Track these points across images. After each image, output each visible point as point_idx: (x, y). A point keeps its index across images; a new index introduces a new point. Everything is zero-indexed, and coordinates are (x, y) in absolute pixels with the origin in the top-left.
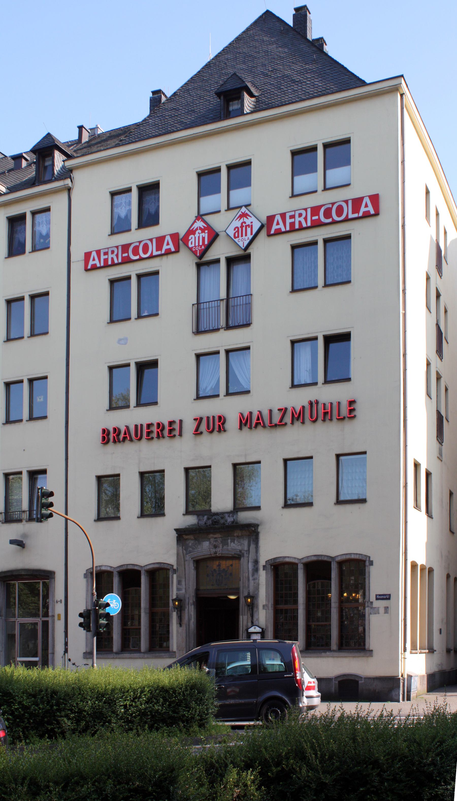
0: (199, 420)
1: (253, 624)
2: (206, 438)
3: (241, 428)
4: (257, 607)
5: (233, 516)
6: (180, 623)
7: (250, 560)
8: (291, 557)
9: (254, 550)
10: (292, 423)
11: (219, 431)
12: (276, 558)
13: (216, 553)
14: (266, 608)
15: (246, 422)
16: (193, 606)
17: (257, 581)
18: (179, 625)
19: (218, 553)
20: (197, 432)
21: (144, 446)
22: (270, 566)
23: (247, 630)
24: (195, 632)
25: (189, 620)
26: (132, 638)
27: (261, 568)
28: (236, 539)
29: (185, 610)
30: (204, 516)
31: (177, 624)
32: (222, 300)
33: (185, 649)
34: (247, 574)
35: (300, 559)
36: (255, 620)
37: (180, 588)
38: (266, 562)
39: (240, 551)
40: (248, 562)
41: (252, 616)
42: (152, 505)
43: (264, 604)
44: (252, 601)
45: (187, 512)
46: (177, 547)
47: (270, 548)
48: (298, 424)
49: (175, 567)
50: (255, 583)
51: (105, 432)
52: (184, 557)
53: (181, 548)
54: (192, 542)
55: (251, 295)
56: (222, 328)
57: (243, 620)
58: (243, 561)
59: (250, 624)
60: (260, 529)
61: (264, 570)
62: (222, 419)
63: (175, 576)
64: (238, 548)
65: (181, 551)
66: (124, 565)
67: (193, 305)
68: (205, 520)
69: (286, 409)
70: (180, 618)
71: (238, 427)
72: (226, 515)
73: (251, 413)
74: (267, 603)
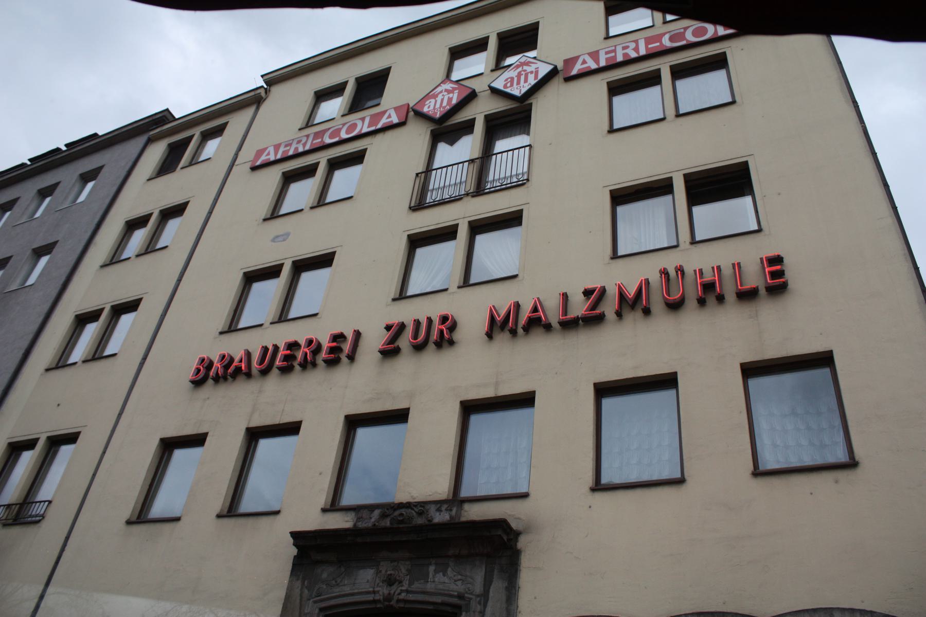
0: (396, 331)
2: (406, 363)
3: (490, 335)
5: (451, 510)
10: (619, 314)
11: (439, 345)
13: (388, 598)
15: (501, 326)
19: (396, 598)
20: (390, 352)
21: (273, 385)
39: (461, 596)
46: (290, 582)
48: (633, 319)
52: (300, 608)
53: (298, 584)
60: (522, 542)
62: (449, 323)
64: (455, 587)
65: (297, 591)
67: (417, 175)
68: (373, 520)
69: (603, 291)
72: (432, 509)
73: (517, 306)
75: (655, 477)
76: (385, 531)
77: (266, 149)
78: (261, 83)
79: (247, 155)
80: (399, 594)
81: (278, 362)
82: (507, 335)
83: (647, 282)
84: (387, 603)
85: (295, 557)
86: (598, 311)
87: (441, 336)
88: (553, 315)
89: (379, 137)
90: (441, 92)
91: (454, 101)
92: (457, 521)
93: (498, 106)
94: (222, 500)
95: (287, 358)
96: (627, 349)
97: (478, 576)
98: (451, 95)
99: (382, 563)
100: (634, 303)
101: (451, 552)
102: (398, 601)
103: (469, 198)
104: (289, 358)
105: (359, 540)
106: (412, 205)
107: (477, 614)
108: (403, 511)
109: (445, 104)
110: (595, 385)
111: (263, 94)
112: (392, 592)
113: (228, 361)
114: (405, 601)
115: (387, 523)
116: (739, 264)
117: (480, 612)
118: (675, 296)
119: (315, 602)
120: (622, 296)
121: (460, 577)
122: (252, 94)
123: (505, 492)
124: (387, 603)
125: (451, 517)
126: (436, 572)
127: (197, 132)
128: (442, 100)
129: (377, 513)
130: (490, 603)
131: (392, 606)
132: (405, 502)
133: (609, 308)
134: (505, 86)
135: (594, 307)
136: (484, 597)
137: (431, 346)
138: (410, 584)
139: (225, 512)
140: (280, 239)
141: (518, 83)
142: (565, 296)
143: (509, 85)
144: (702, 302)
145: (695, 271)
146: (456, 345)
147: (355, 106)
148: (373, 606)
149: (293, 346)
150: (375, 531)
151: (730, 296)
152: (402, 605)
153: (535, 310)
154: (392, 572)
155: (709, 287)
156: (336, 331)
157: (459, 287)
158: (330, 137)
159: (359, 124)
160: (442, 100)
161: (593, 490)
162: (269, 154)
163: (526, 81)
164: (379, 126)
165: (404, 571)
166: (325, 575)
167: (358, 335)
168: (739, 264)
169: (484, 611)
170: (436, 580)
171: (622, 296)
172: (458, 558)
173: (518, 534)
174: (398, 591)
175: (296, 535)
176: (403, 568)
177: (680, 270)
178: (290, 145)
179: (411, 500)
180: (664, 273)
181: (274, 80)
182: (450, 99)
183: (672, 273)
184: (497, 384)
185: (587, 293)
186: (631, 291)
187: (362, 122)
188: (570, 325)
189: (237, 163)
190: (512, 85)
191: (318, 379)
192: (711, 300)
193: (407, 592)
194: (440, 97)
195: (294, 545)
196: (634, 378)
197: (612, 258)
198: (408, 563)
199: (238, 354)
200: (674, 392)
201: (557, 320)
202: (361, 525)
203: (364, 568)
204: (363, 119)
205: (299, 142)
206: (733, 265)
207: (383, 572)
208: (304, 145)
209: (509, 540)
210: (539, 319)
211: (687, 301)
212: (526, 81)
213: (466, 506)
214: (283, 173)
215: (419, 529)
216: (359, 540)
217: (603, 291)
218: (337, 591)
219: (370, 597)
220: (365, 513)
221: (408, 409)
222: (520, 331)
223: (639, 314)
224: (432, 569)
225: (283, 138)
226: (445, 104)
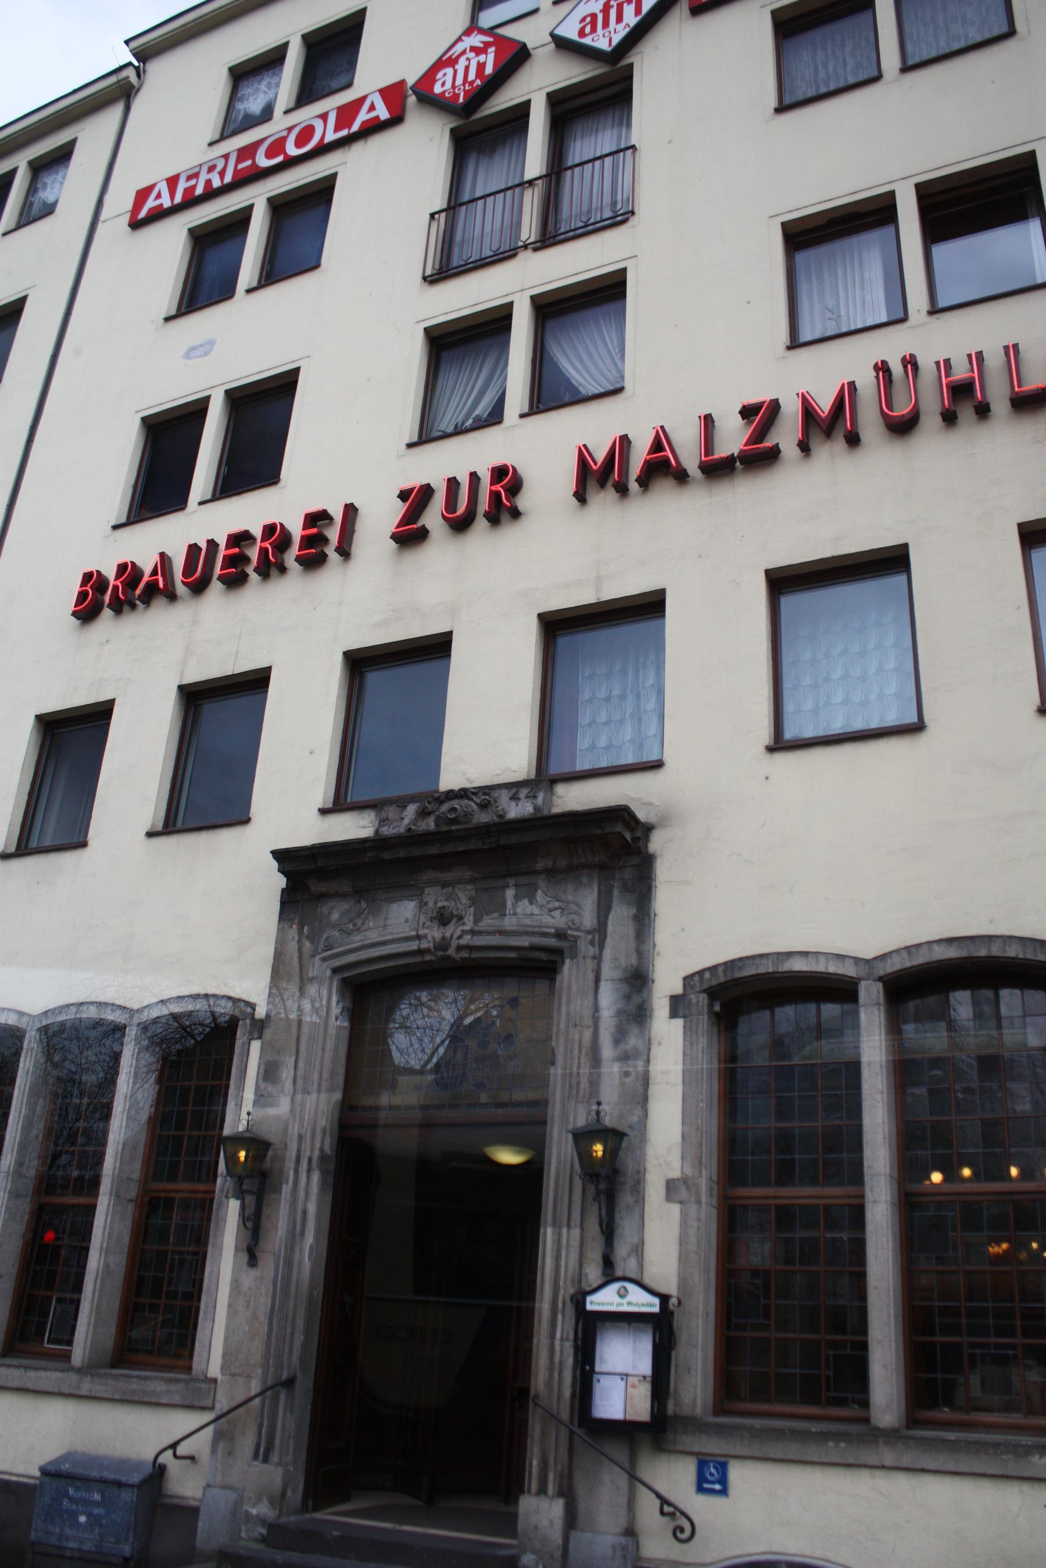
0: (416, 499)
1: (610, 1276)
2: (441, 550)
3: (581, 496)
4: (638, 1188)
5: (535, 797)
6: (251, 1252)
7: (607, 971)
8: (817, 954)
9: (630, 929)
10: (805, 447)
11: (494, 519)
12: (741, 959)
13: (443, 945)
14: (683, 1194)
15: (599, 476)
16: (316, 1177)
17: (640, 1064)
18: (245, 1257)
19: (454, 944)
20: (409, 536)
22: (704, 999)
23: (579, 1300)
24: (319, 1292)
25: (294, 1236)
26: (59, 1301)
27: (661, 1008)
28: (542, 884)
29: (278, 1190)
30: (404, 807)
31: (237, 1249)
32: (531, 183)
33: (259, 1371)
34: (588, 1034)
35: (867, 962)
36: (621, 1250)
37: (271, 1102)
38: (687, 980)
39: (560, 935)
40: (597, 980)
41: (609, 1232)
42: (207, 788)
43: (676, 1174)
44: (612, 1153)
45: (340, 803)
46: (281, 931)
47: (709, 914)
48: (830, 454)
49: (261, 1012)
50: (627, 1074)
51: (93, 582)
53: (293, 932)
54: (344, 906)
55: (633, 147)
56: (525, 247)
57: (561, 1248)
58: (571, 975)
59: (593, 1273)
60: (656, 843)
61: (674, 1015)
62: (507, 480)
63: (256, 1046)
64: (550, 921)
65: (292, 946)
66: (68, 1006)
67: (432, 216)
68: (406, 821)
69: (774, 407)
70: (254, 1227)
71: (572, 487)
72: (504, 796)
73: (625, 441)
74: (689, 1171)
75: (874, 724)
76: (427, 837)
77: (151, 188)
78: (126, 56)
79: (120, 201)
80: (460, 937)
81: (217, 571)
82: (610, 494)
83: (852, 385)
84: (440, 953)
85: (283, 891)
86: (768, 443)
87: (501, 498)
88: (688, 452)
89: (358, 149)
90: (464, 52)
91: (489, 70)
92: (546, 813)
93: (569, 73)
94: (152, 808)
95: (231, 561)
96: (819, 507)
97: (586, 901)
98: (482, 58)
99: (427, 891)
100: (831, 425)
101: (540, 865)
102: (460, 948)
103: (529, 253)
104: (236, 561)
105: (387, 856)
106: (428, 272)
107: (589, 961)
108: (455, 803)
109: (472, 76)
110: (768, 572)
111: (133, 79)
112: (448, 934)
113: (129, 572)
114: (471, 948)
115: (429, 824)
116: (1016, 346)
117: (594, 957)
118: (902, 409)
119: (324, 960)
120: (808, 412)
121: (557, 904)
122: (113, 79)
123: (623, 762)
124: (440, 953)
125: (536, 808)
126: (517, 898)
127: (21, 161)
128: (467, 68)
129: (412, 809)
130: (609, 942)
131: (449, 956)
132: (456, 788)
133: (786, 435)
134: (582, 33)
135: (759, 436)
136: (600, 931)
137: (481, 523)
138: (476, 922)
139: (160, 827)
140: (197, 353)
141: (606, 24)
142: (708, 421)
143: (588, 30)
144: (949, 418)
145: (938, 363)
146: (523, 518)
147: (307, 93)
148: (418, 959)
149: (241, 539)
150: (412, 838)
151: (1000, 405)
152: (465, 954)
153: (657, 446)
154: (446, 904)
155: (961, 391)
156: (314, 507)
157: (522, 416)
158: (269, 155)
159: (319, 125)
160: (467, 68)
161: (771, 749)
162: (159, 196)
163: (619, 19)
164: (356, 127)
165: (464, 900)
166: (335, 916)
167: (350, 511)
168: (1016, 346)
169: (601, 954)
170: (519, 910)
171: (808, 412)
172: (553, 874)
173: (649, 828)
174: (458, 933)
175: (280, 855)
176: (463, 896)
177: (910, 363)
178: (196, 176)
179: (468, 785)
180: (883, 369)
181: (149, 49)
182: (481, 67)
183: (897, 368)
184: (599, 581)
185: (748, 412)
186: (824, 404)
187: (321, 116)
188: (718, 469)
189: (102, 218)
190: (594, 30)
191: (293, 588)
192: (966, 413)
193: (473, 932)
194: (461, 66)
195: (279, 871)
196: (833, 558)
197: (789, 348)
198: (469, 887)
199: (147, 563)
200: (903, 578)
201: (697, 463)
202: (386, 831)
203: (398, 899)
204: (324, 117)
205: (211, 169)
206: (1006, 348)
207: (431, 904)
208: (222, 174)
209: (636, 839)
210: (666, 462)
211: (923, 418)
212: (619, 19)
213: (560, 789)
214: (191, 231)
215: (485, 831)
216: (387, 856)
217: (774, 407)
218: (357, 940)
219: (414, 946)
220: (392, 812)
221: (450, 634)
222: (634, 486)
223: (839, 444)
224: (510, 893)
225: (181, 162)
226: (472, 76)
